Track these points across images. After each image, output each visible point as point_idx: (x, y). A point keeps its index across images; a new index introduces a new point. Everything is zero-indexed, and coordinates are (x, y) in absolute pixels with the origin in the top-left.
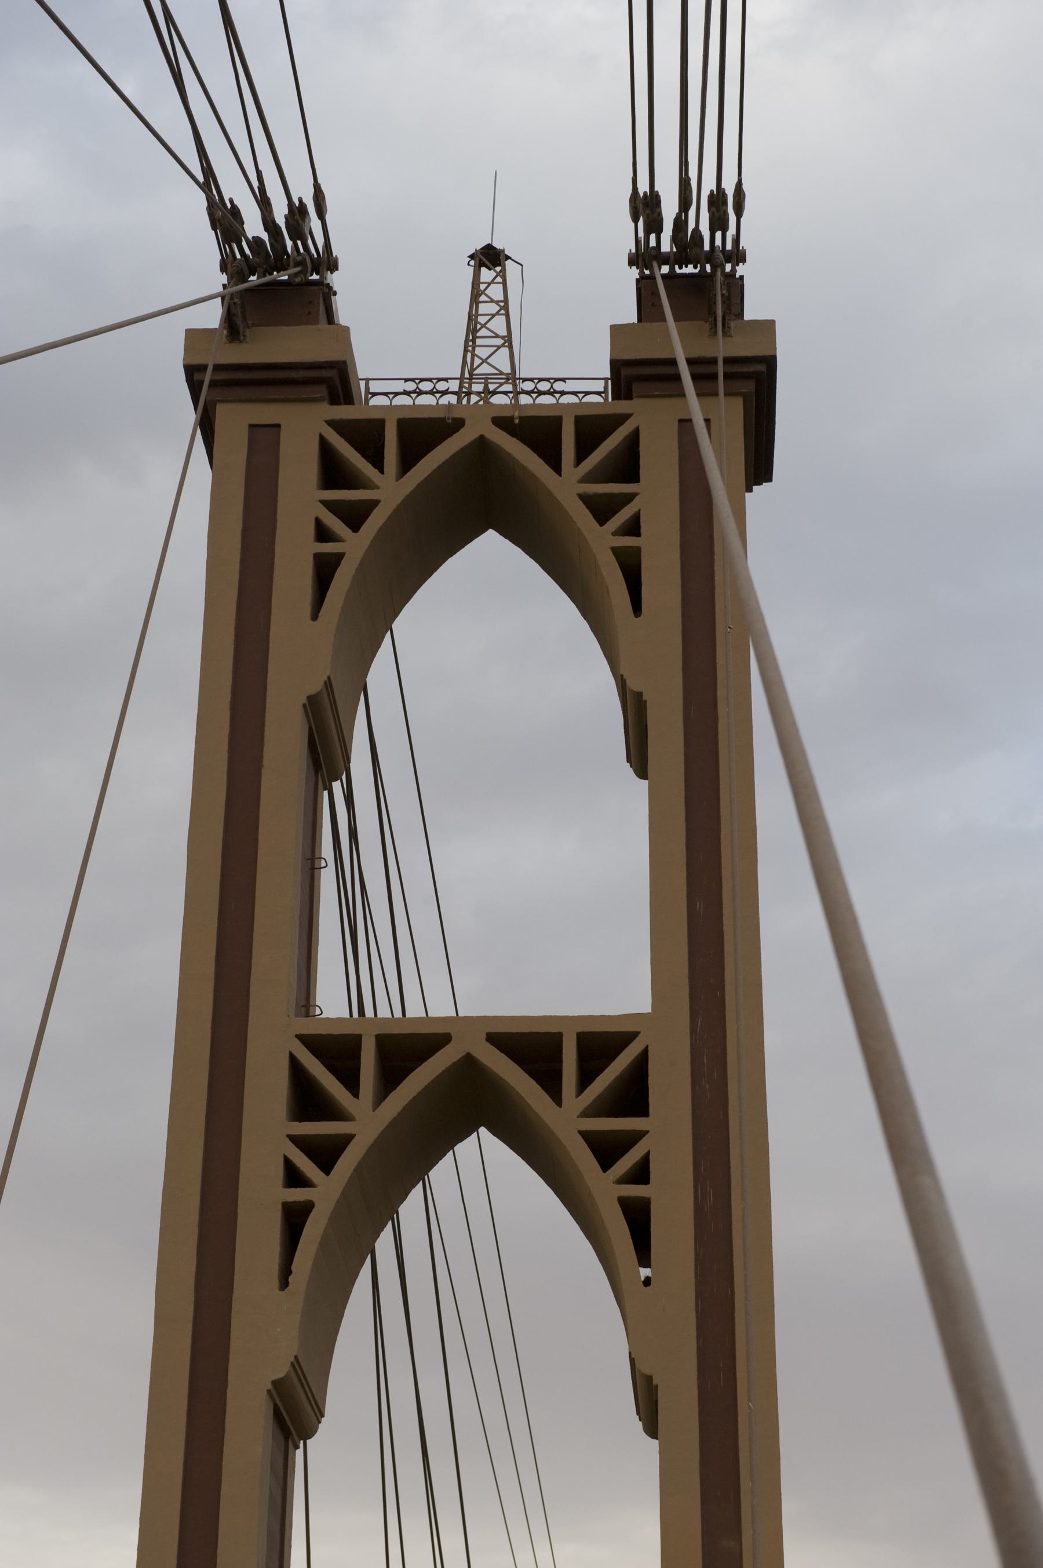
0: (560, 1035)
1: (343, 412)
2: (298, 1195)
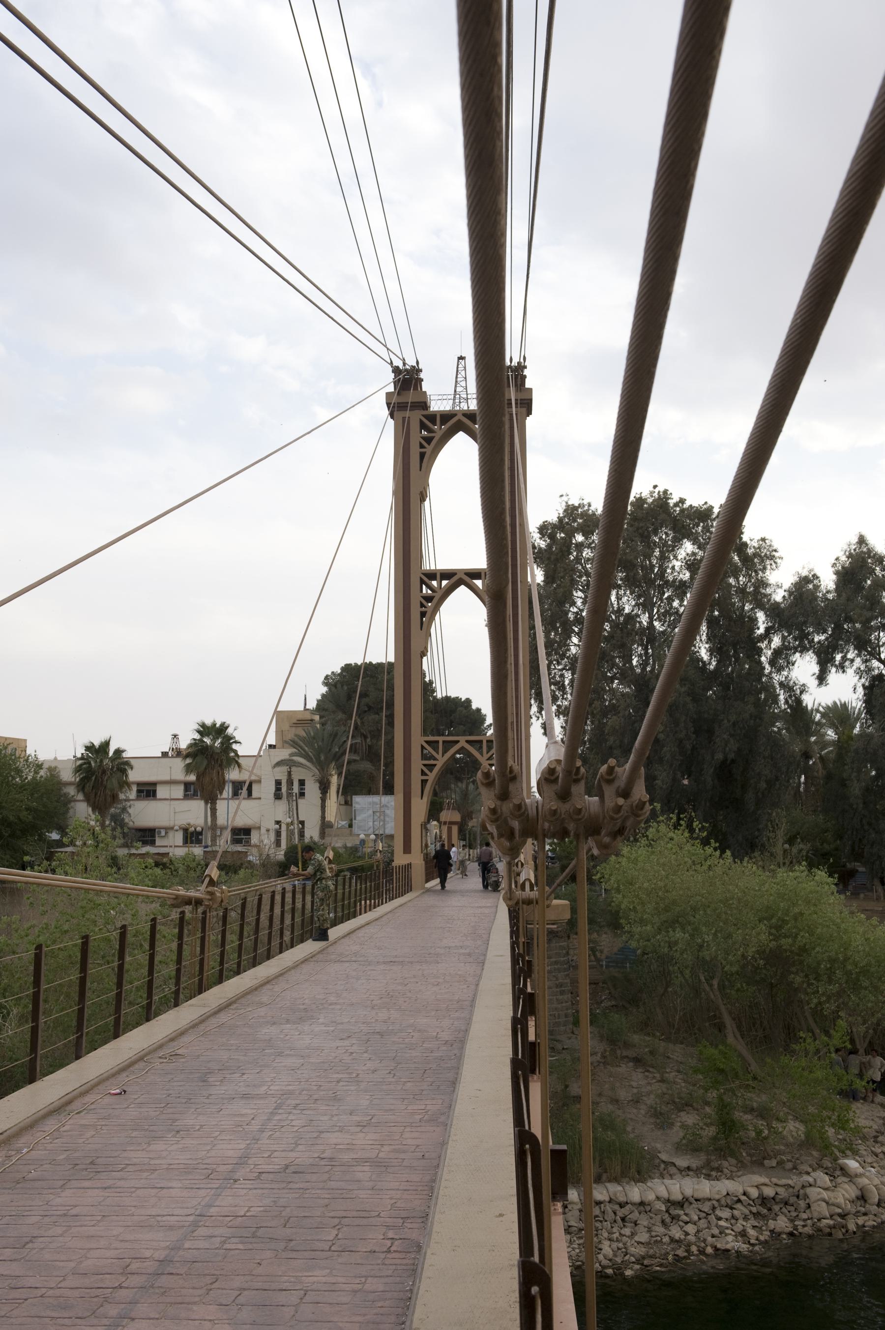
0: (436, 415)
1: (425, 413)
2: (425, 778)
